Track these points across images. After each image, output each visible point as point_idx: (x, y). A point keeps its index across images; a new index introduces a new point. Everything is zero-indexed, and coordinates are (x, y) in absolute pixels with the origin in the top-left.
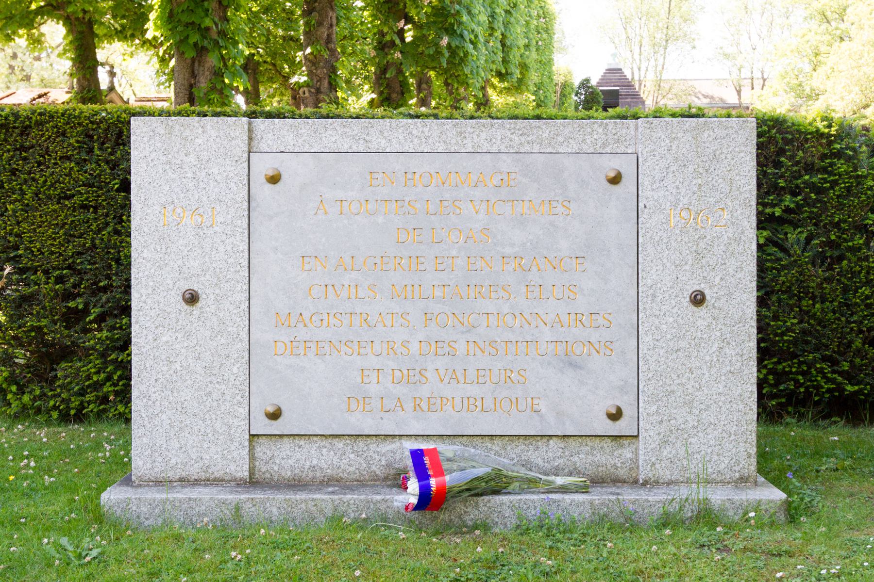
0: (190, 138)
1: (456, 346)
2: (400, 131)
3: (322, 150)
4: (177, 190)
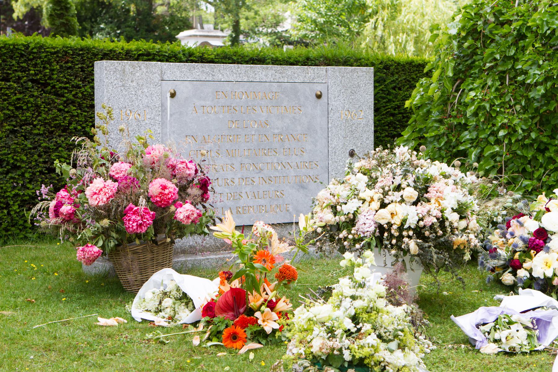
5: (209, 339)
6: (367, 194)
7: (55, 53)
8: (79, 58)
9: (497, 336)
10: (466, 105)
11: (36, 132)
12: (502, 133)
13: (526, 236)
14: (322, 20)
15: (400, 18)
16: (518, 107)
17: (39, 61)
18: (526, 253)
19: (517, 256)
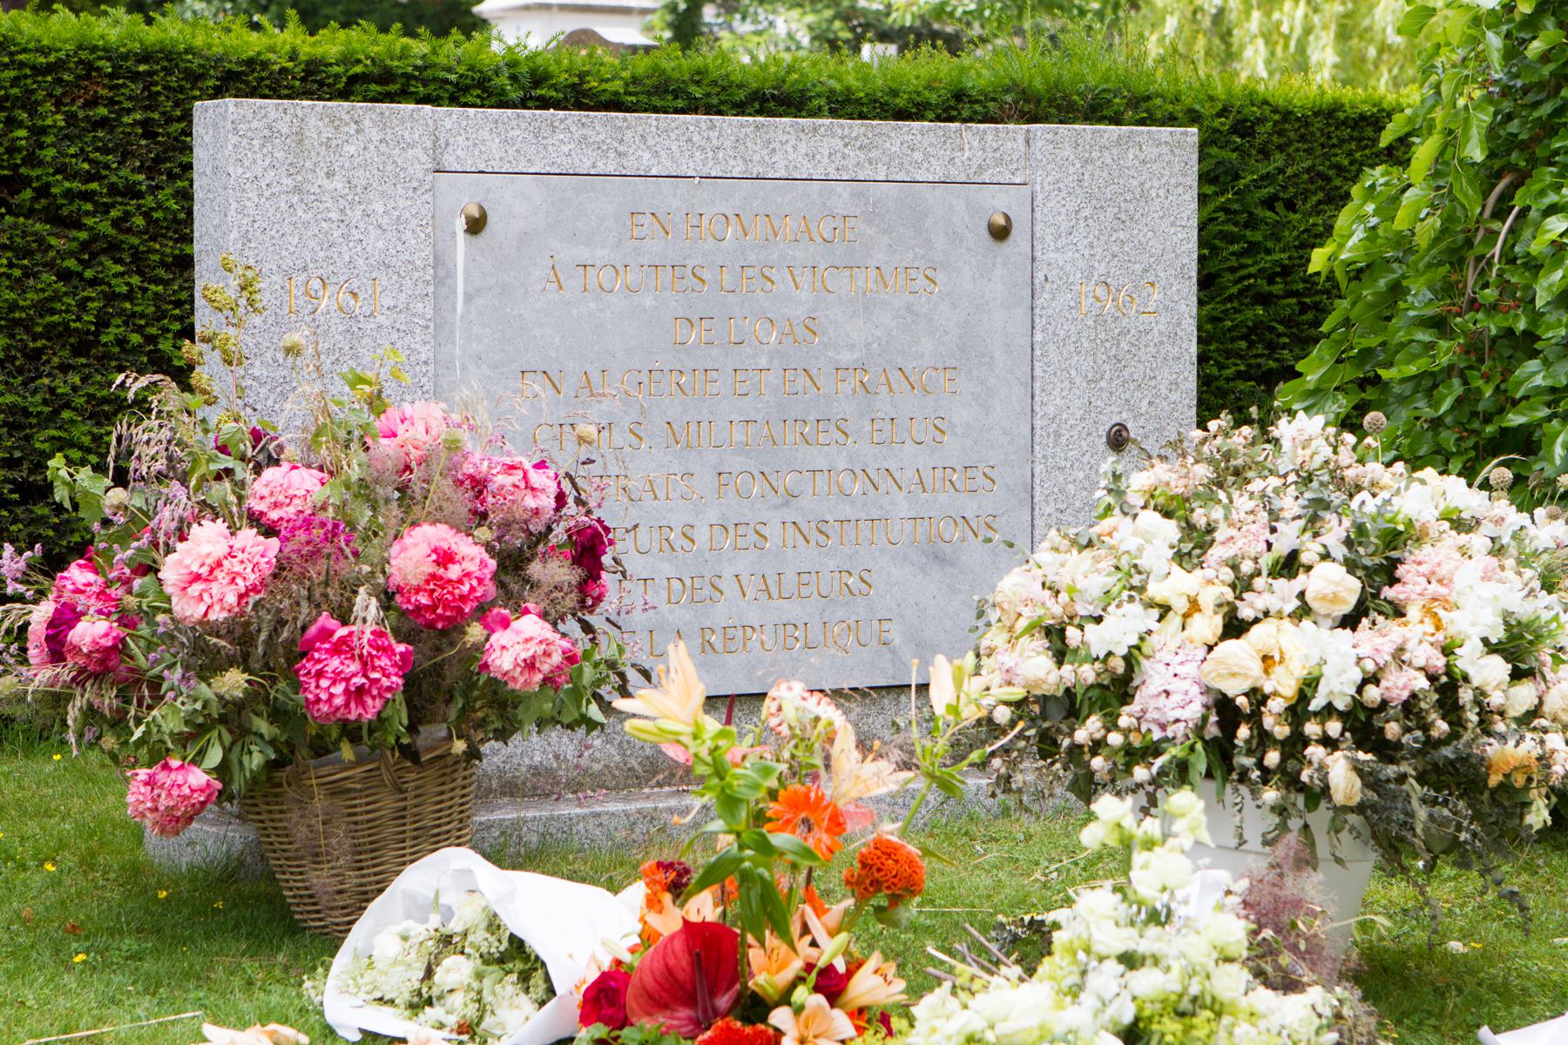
0: (334, 143)
1: (765, 531)
2: (673, 137)
3: (548, 169)
4: (312, 244)
6: (1174, 585)
7: (49, 69)
8: (136, 88)
10: (1534, 267)
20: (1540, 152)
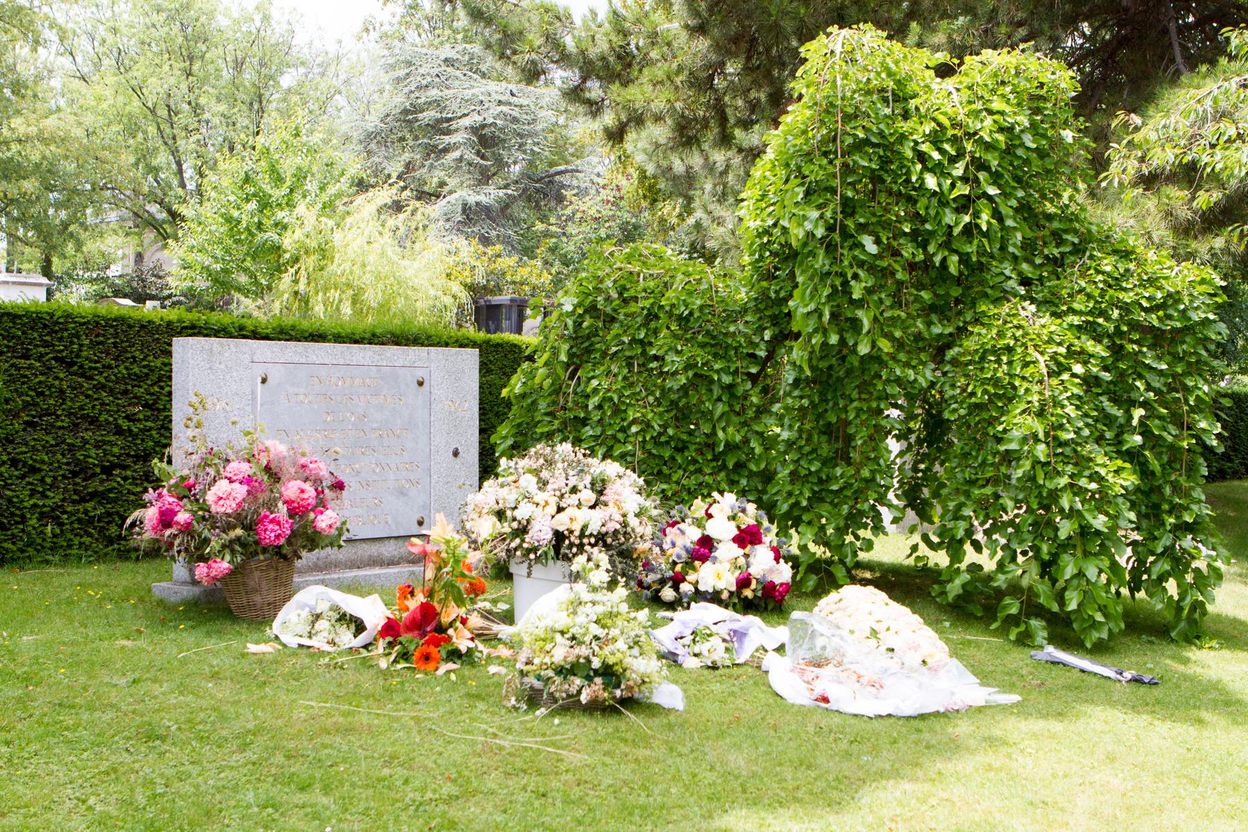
5: (395, 661)
6: (540, 497)
7: (84, 324)
8: (112, 331)
9: (697, 649)
10: (588, 397)
11: (60, 424)
12: (634, 429)
13: (689, 545)
14: (218, 267)
15: (332, 268)
16: (651, 399)
17: (66, 334)
18: (689, 565)
19: (678, 568)
20: (584, 358)
